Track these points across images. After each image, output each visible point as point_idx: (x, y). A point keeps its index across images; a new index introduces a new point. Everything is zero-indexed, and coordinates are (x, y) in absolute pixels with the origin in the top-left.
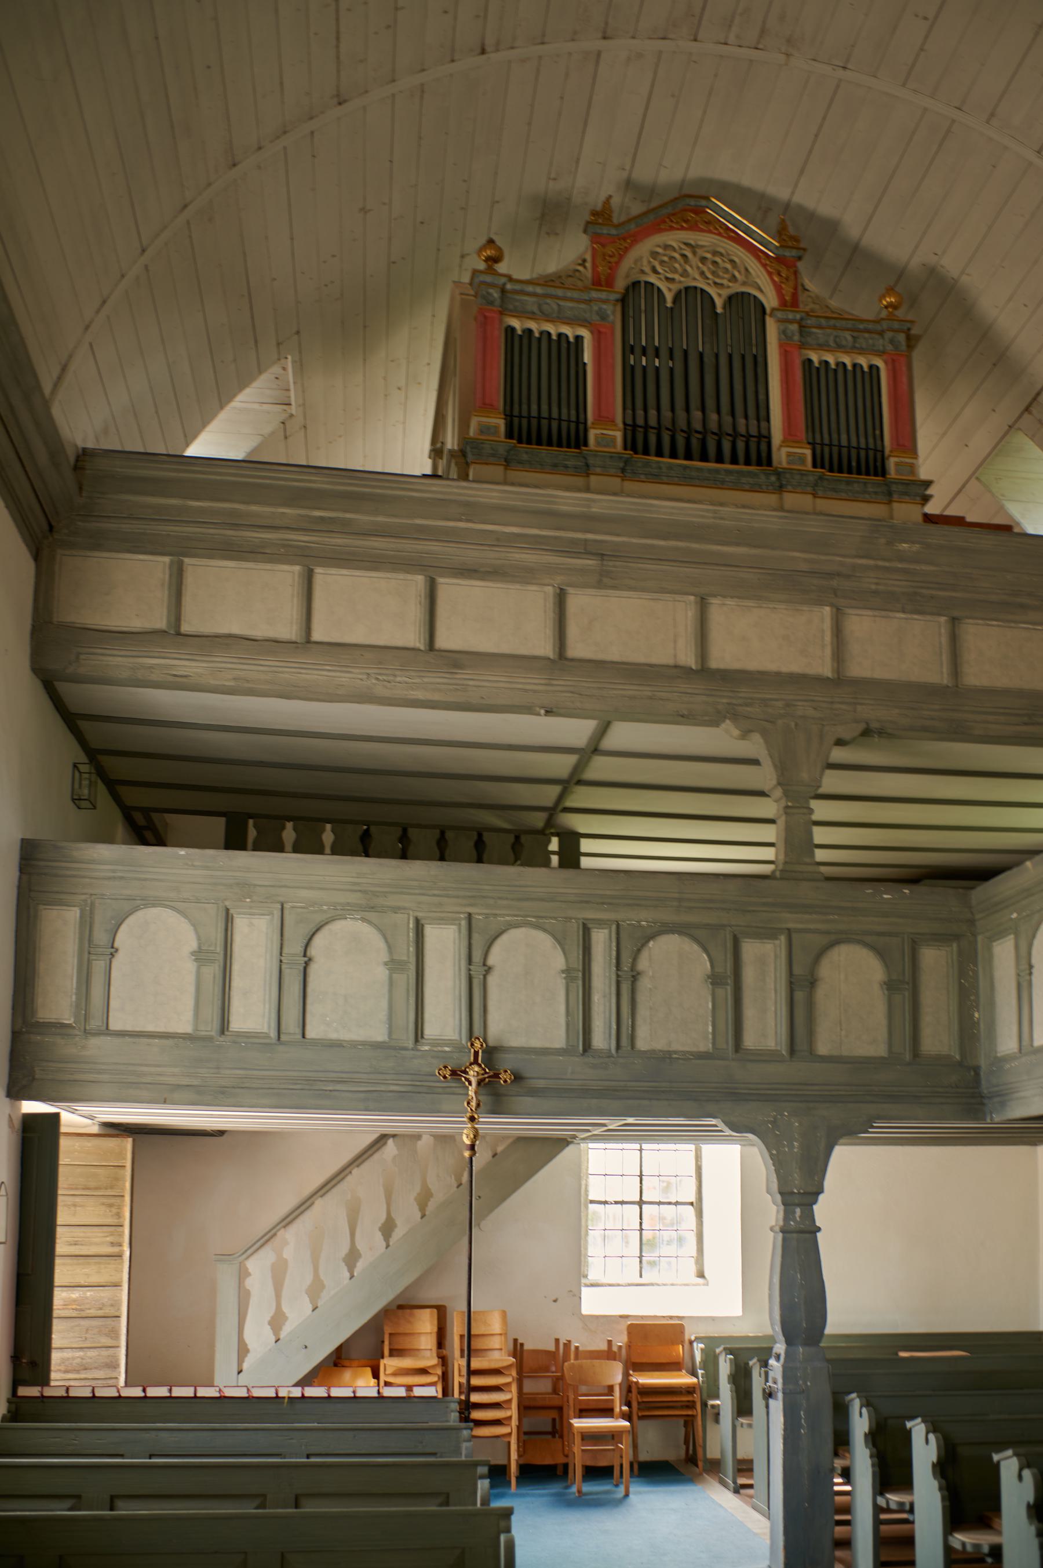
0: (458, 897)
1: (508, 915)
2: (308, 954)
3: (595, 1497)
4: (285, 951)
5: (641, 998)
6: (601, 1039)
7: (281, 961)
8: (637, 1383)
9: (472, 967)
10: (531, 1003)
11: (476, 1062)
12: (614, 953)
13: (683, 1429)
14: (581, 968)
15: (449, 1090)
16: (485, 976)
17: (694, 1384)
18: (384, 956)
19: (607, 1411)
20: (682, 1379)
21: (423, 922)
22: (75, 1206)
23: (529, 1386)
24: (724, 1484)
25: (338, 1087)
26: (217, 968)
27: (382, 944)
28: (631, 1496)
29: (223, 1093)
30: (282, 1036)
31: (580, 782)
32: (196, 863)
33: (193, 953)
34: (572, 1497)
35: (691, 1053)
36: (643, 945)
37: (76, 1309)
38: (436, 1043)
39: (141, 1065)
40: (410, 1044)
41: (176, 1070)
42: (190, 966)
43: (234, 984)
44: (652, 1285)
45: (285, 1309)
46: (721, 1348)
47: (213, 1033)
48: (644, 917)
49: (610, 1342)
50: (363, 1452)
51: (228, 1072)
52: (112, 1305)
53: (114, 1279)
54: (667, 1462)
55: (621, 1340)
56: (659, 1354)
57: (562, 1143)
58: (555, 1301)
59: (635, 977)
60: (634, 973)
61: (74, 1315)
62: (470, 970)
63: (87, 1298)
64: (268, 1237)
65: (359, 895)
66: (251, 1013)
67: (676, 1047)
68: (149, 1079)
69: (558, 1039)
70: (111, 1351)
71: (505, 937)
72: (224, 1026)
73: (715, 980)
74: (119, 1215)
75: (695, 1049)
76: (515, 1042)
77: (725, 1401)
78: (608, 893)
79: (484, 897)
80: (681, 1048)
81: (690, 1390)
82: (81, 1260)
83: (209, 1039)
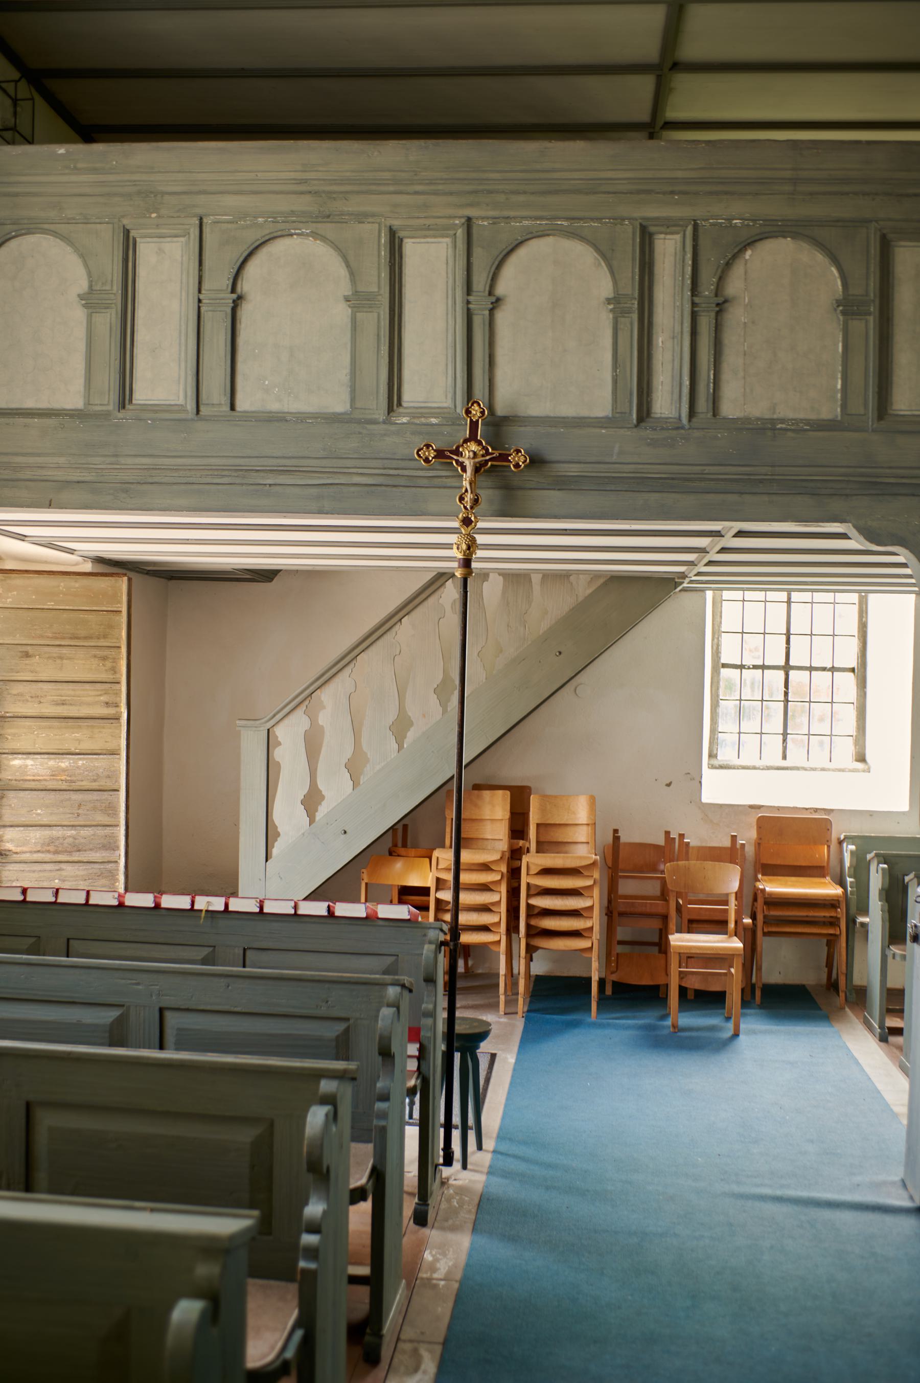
0: (451, 194)
1: (525, 218)
2: (239, 289)
3: (694, 1034)
4: (206, 286)
5: (732, 338)
6: (666, 401)
7: (200, 301)
8: (763, 891)
9: (471, 298)
10: (560, 355)
11: (473, 437)
12: (689, 270)
13: (826, 948)
14: (636, 295)
15: (437, 481)
16: (492, 311)
17: (838, 896)
18: (345, 288)
19: (717, 925)
20: (828, 889)
21: (401, 234)
22: (61, 658)
23: (627, 887)
24: (870, 1028)
25: (282, 479)
26: (114, 315)
27: (343, 272)
28: (742, 1037)
29: (126, 491)
30: (202, 408)
31: (677, 66)
32: (80, 165)
33: (81, 297)
34: (665, 1032)
35: (808, 422)
36: (735, 256)
37: (66, 781)
38: (420, 412)
39: (17, 454)
40: (381, 414)
41: (62, 460)
42: (80, 314)
43: (138, 337)
44: (797, 768)
45: (321, 786)
46: (872, 855)
47: (111, 408)
48: (738, 211)
49: (734, 838)
50: (238, 1009)
51: (129, 461)
52: (108, 777)
53: (110, 746)
54: (804, 986)
55: (748, 836)
56: (798, 855)
57: (666, 585)
58: (669, 785)
59: (721, 306)
60: (720, 300)
61: (64, 787)
62: (468, 302)
63: (78, 767)
64: (306, 698)
65: (308, 198)
66: (161, 378)
67: (784, 412)
68: (28, 474)
69: (600, 403)
70: (108, 831)
71: (522, 252)
72: (125, 397)
73: (848, 307)
74: (114, 670)
75: (813, 416)
76: (536, 409)
77: (874, 919)
78: (679, 174)
79: (490, 192)
80: (791, 415)
81: (831, 904)
82: (71, 723)
83: (106, 415)
